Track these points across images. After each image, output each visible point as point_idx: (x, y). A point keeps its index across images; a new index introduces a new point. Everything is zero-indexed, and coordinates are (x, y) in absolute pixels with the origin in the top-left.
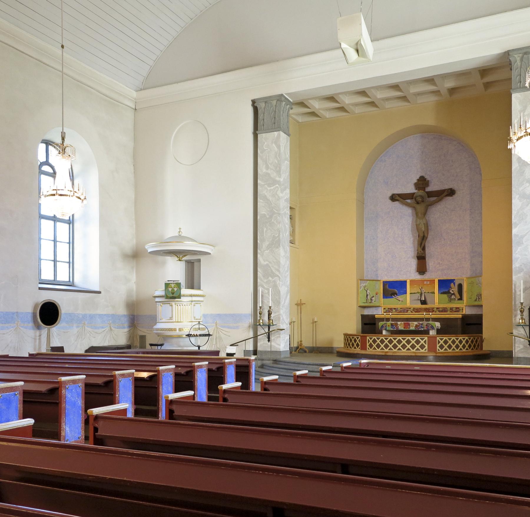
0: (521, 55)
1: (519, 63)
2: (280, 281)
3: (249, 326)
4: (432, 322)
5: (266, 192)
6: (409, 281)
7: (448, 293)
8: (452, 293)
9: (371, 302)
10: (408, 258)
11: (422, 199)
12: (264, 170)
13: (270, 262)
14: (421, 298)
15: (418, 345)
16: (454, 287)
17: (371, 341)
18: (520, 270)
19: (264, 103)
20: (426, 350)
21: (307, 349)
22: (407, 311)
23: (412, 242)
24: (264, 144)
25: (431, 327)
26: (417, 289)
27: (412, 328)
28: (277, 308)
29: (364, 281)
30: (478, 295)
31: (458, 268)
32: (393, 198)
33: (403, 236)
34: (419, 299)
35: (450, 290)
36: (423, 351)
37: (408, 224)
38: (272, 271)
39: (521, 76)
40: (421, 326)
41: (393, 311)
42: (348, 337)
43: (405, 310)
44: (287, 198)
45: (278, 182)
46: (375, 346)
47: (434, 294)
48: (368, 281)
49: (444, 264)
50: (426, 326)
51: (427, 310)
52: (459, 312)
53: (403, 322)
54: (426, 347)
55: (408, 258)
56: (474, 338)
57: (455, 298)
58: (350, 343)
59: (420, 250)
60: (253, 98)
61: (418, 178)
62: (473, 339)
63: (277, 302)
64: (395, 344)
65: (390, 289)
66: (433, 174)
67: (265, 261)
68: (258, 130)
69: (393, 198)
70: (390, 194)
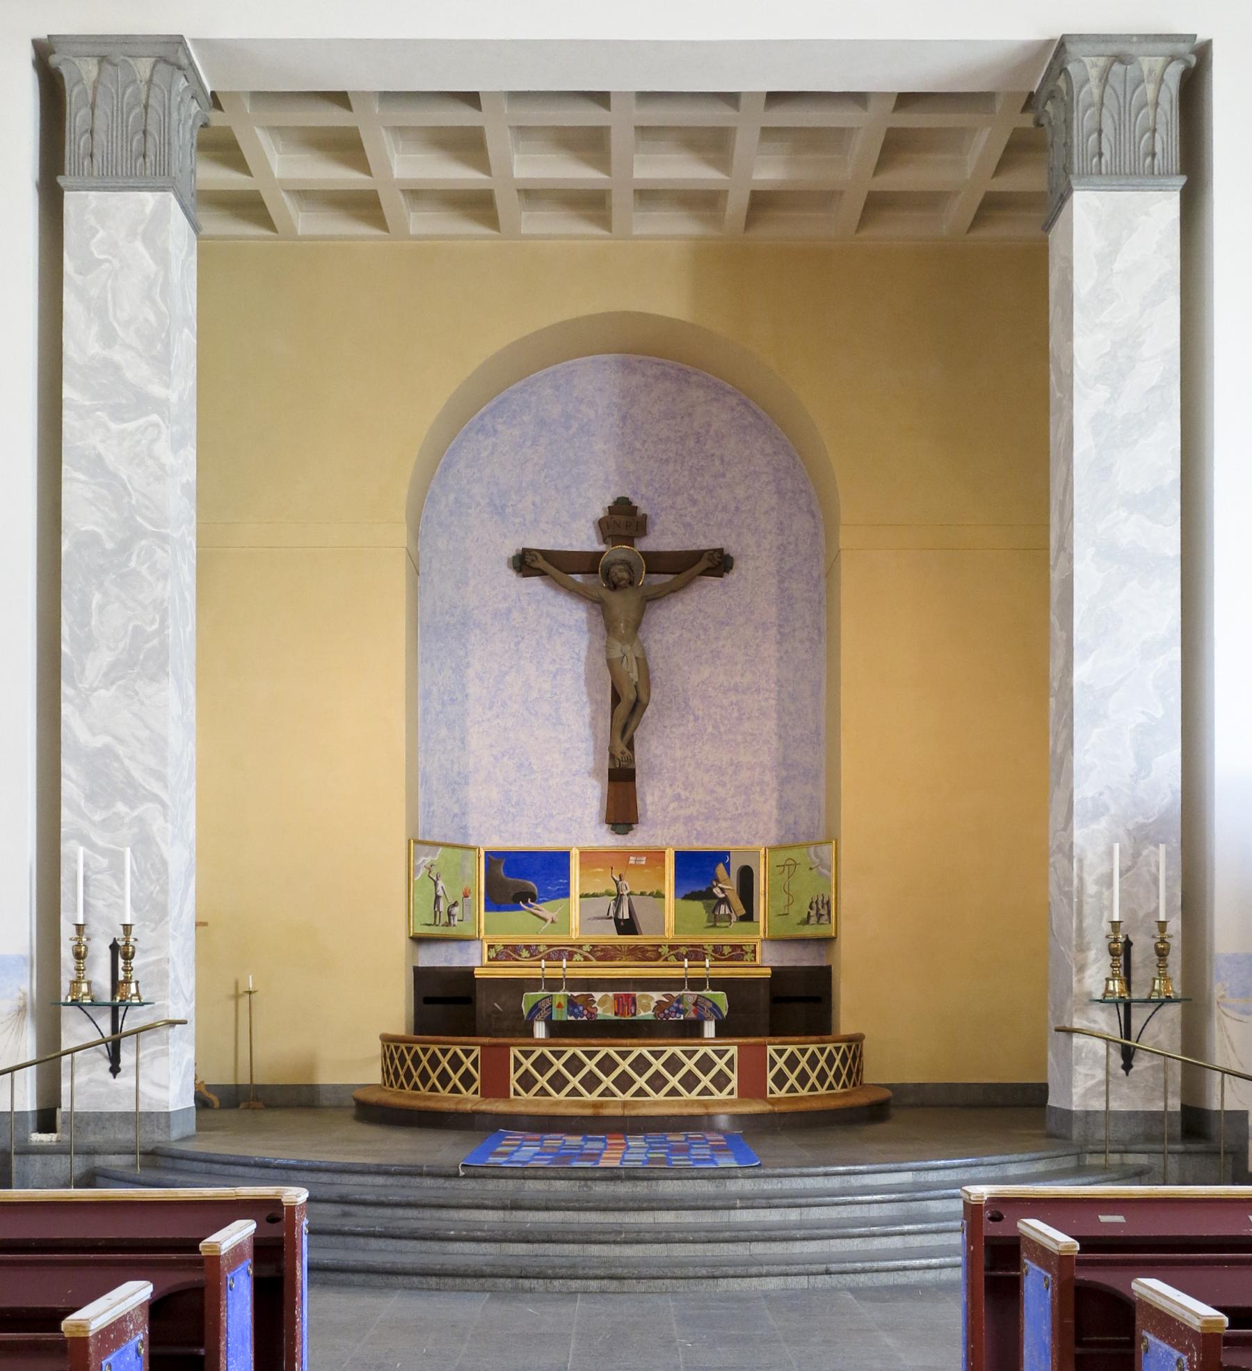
0: (1102, 62)
1: (1093, 87)
2: (166, 821)
3: (21, 1010)
4: (710, 992)
5: (103, 441)
6: (578, 852)
7: (706, 895)
8: (722, 896)
9: (448, 924)
10: (574, 775)
11: (630, 574)
12: (94, 348)
13: (121, 741)
14: (617, 913)
15: (705, 1076)
16: (726, 876)
17: (527, 1064)
18: (1099, 811)
19: (95, 61)
20: (731, 1093)
21: (215, 1094)
22: (570, 957)
23: (587, 720)
24: (93, 236)
25: (711, 1009)
26: (603, 883)
27: (642, 1014)
28: (153, 930)
29: (427, 848)
30: (817, 903)
31: (740, 814)
32: (525, 563)
33: (556, 698)
34: (611, 914)
35: (714, 887)
36: (723, 1096)
37: (576, 656)
38: (128, 774)
39: (1103, 135)
40: (676, 1005)
41: (520, 956)
42: (403, 1046)
43: (558, 953)
44: (188, 480)
45: (160, 405)
46: (543, 1081)
47: (662, 899)
48: (441, 849)
49: (694, 801)
50: (693, 1007)
51: (640, 954)
52: (742, 960)
53: (611, 994)
54: (734, 1083)
55: (574, 775)
56: (838, 1049)
57: (729, 915)
58: (412, 1067)
59: (621, 746)
60: (42, 34)
61: (609, 501)
62: (834, 1052)
63: (157, 911)
64: (690, 1072)
65: (510, 879)
66: (659, 496)
67: (94, 734)
68: (67, 173)
69: (525, 563)
70: (511, 548)
